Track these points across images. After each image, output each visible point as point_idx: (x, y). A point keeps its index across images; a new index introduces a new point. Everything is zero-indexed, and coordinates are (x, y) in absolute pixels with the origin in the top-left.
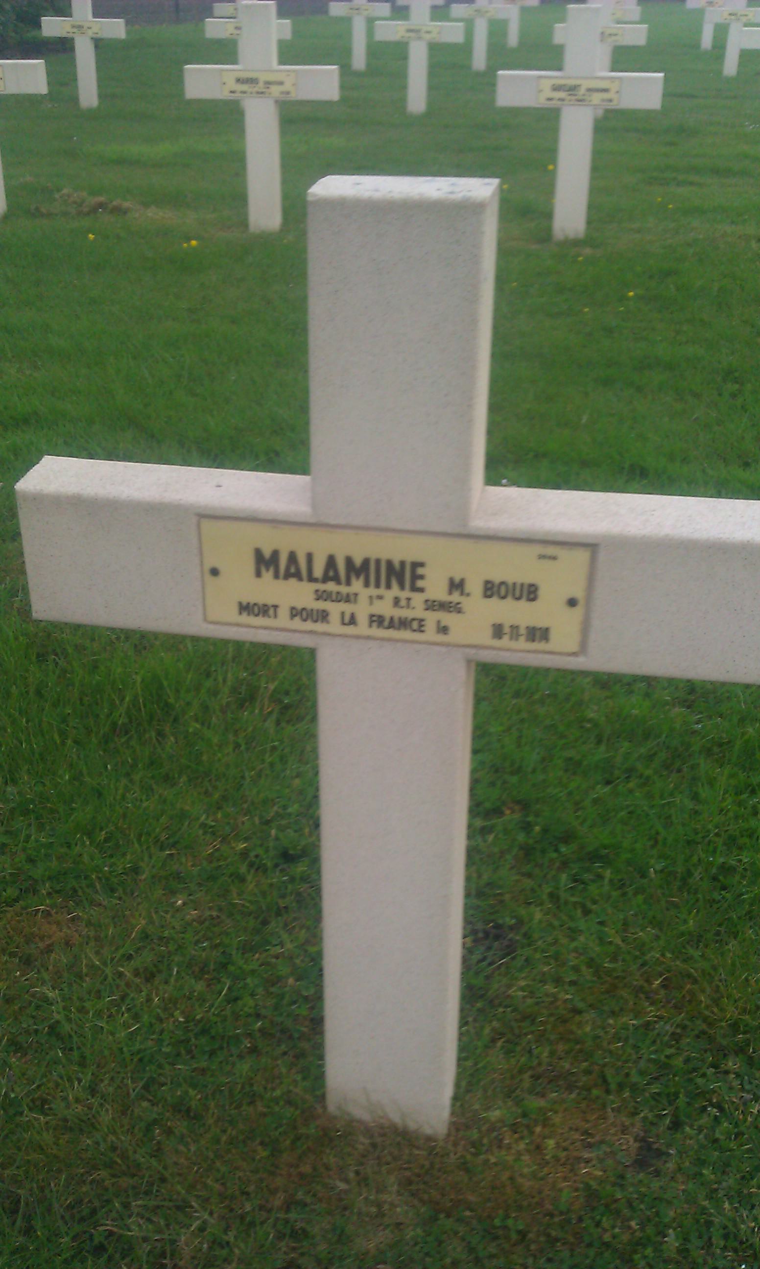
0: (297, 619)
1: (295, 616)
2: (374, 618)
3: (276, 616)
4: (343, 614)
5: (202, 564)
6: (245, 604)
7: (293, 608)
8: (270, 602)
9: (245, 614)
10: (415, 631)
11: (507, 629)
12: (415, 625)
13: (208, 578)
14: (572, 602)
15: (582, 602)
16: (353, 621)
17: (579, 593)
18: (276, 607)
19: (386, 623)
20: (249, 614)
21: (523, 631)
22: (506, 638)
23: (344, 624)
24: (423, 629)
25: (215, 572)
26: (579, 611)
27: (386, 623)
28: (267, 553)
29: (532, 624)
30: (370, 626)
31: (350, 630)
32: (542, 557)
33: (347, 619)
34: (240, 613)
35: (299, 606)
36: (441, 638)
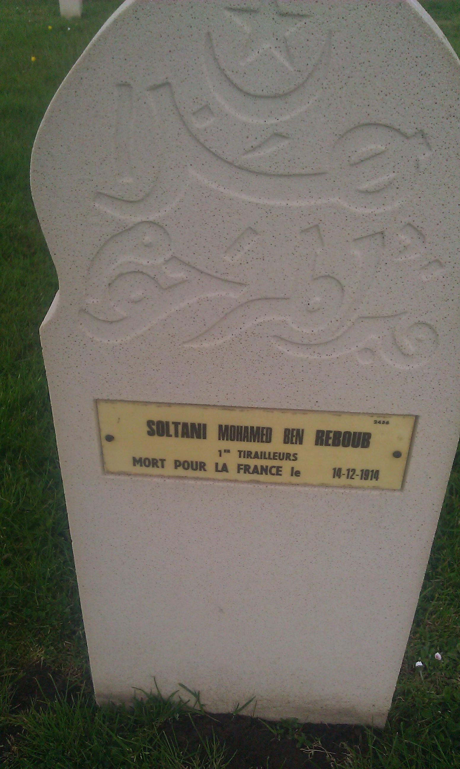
0: (180, 469)
1: (179, 466)
2: (241, 467)
3: (163, 467)
4: (217, 464)
5: (100, 430)
6: (138, 458)
7: (176, 461)
8: (158, 457)
9: (138, 466)
10: (274, 474)
11: (344, 471)
12: (274, 471)
13: (105, 443)
14: (397, 455)
15: (404, 455)
16: (225, 468)
17: (403, 447)
18: (163, 461)
19: (253, 456)
20: (141, 466)
21: (358, 472)
22: (343, 478)
23: (217, 470)
24: (280, 473)
25: (110, 438)
26: (401, 462)
27: (253, 456)
28: (138, 458)
29: (365, 468)
30: (239, 472)
31: (223, 475)
32: (376, 422)
33: (220, 468)
34: (134, 465)
35: (182, 460)
36: (294, 479)
